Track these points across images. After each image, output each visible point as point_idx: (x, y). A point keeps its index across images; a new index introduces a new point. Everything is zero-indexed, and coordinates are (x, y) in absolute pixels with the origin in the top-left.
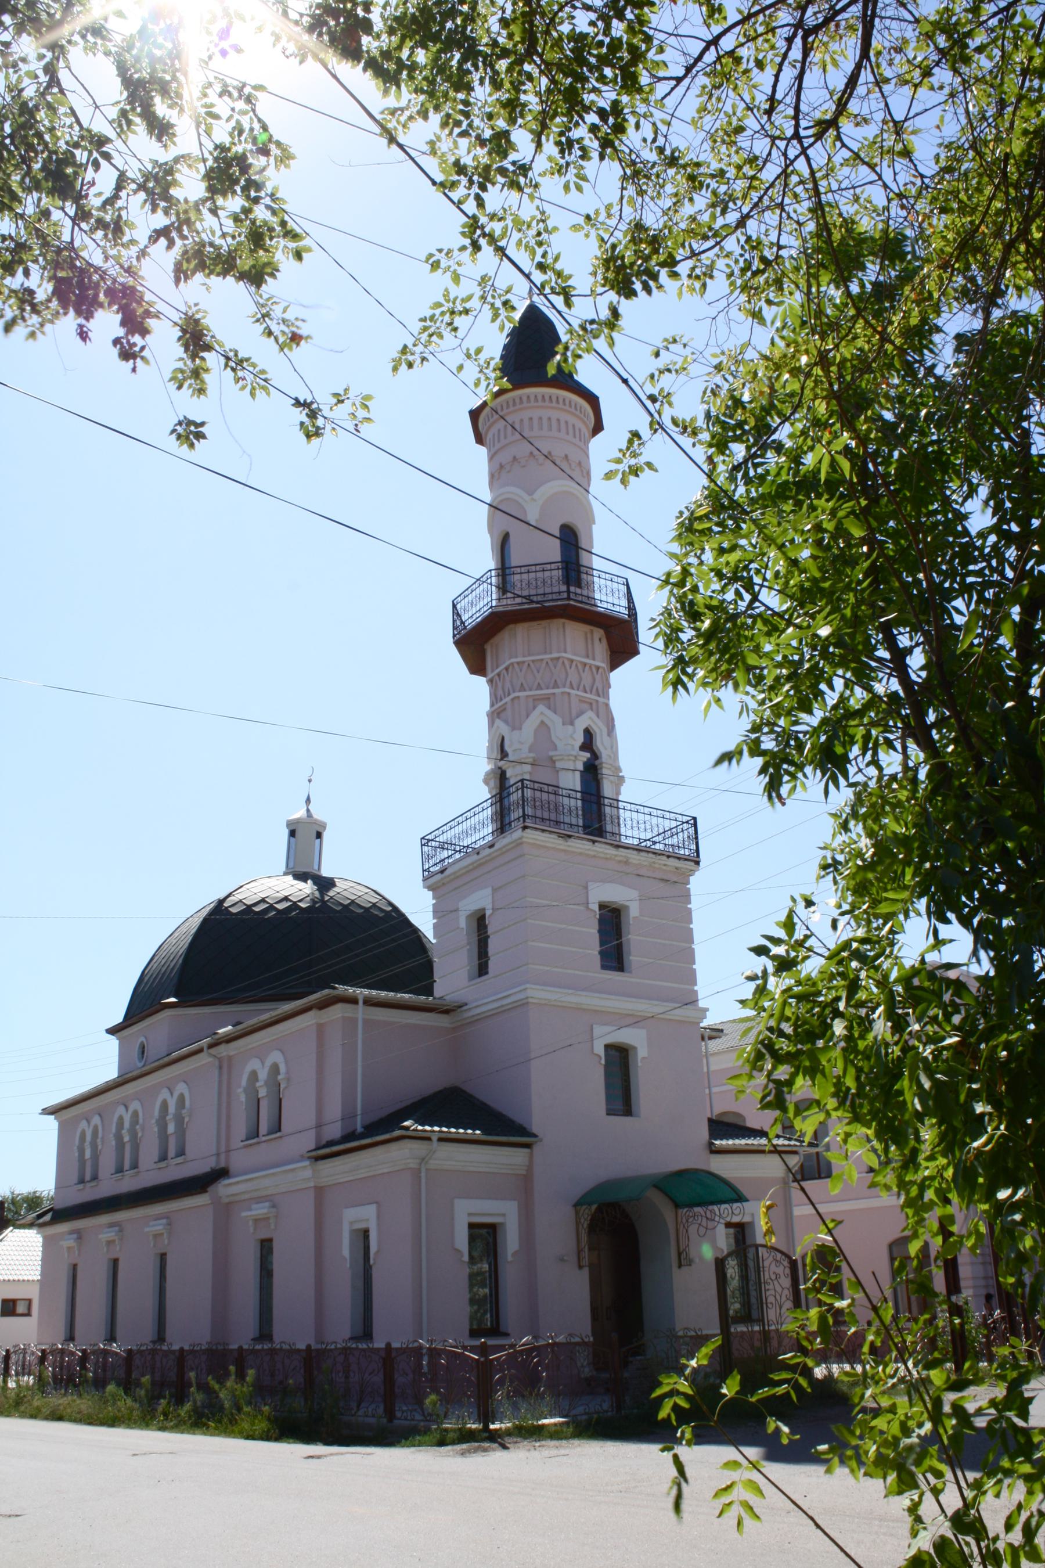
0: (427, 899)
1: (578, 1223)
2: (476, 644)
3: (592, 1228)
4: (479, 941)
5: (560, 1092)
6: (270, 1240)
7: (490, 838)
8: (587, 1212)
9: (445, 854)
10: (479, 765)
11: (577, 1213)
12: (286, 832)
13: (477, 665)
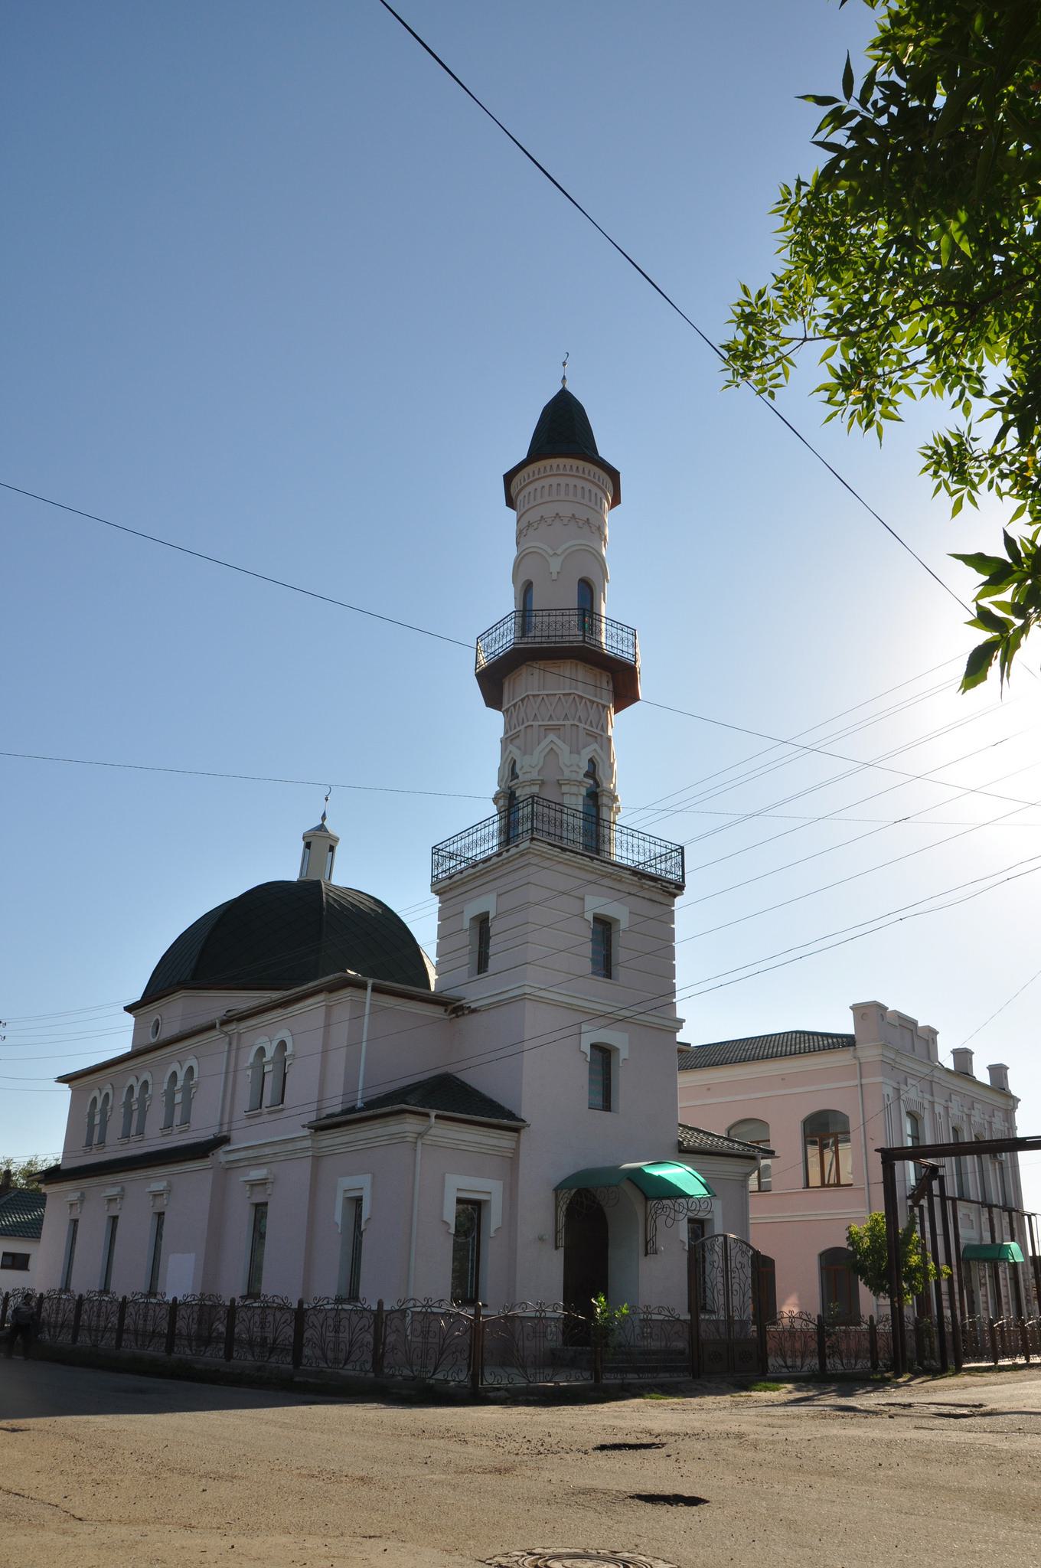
0: (433, 903)
1: (557, 1206)
2: (494, 681)
3: (570, 1213)
4: (481, 928)
5: (545, 1082)
6: (266, 1204)
7: (496, 849)
8: (566, 1197)
9: (453, 863)
10: (491, 784)
11: (557, 1197)
12: (302, 844)
13: (493, 697)
